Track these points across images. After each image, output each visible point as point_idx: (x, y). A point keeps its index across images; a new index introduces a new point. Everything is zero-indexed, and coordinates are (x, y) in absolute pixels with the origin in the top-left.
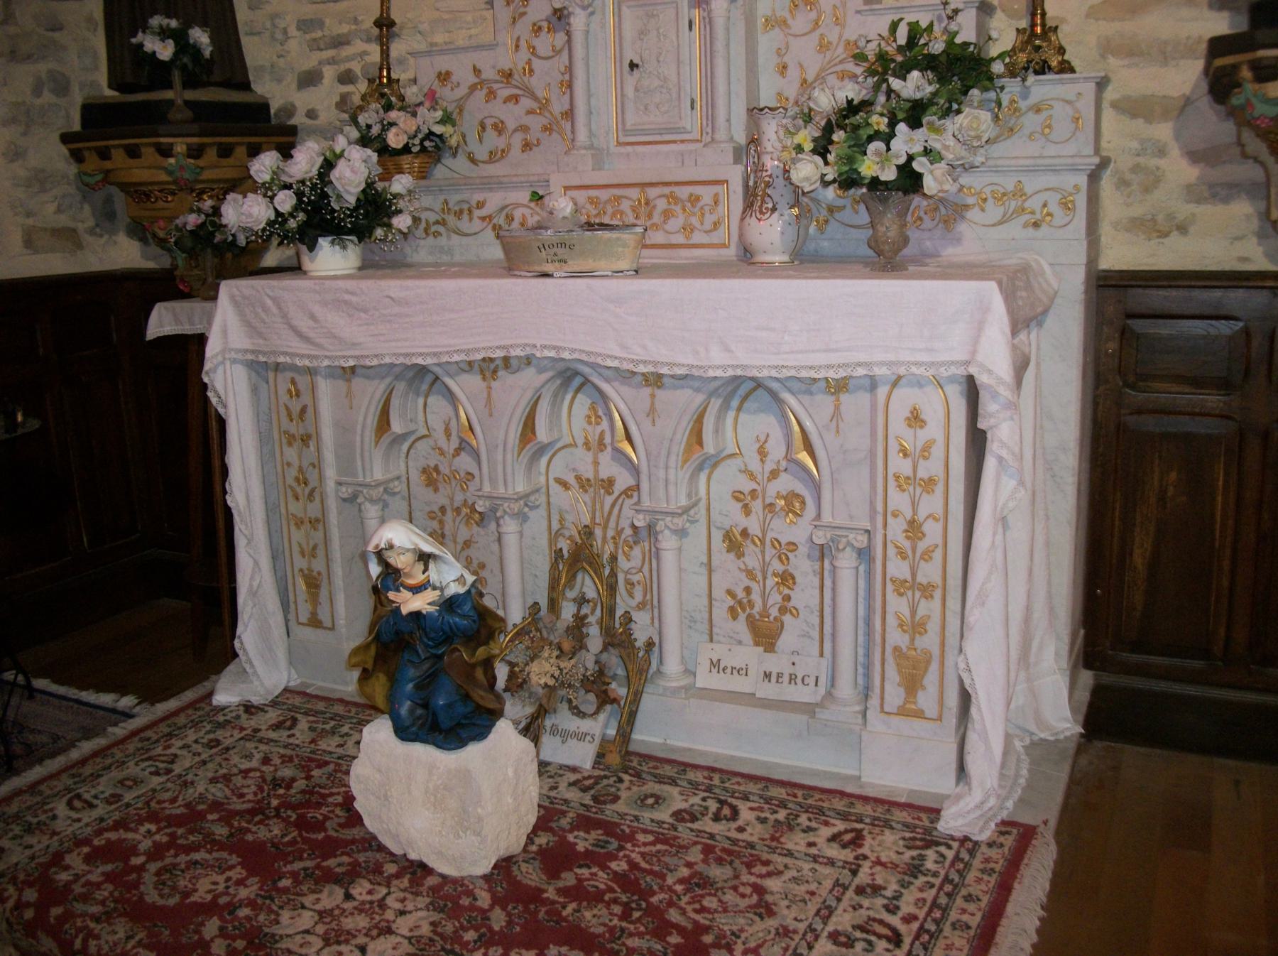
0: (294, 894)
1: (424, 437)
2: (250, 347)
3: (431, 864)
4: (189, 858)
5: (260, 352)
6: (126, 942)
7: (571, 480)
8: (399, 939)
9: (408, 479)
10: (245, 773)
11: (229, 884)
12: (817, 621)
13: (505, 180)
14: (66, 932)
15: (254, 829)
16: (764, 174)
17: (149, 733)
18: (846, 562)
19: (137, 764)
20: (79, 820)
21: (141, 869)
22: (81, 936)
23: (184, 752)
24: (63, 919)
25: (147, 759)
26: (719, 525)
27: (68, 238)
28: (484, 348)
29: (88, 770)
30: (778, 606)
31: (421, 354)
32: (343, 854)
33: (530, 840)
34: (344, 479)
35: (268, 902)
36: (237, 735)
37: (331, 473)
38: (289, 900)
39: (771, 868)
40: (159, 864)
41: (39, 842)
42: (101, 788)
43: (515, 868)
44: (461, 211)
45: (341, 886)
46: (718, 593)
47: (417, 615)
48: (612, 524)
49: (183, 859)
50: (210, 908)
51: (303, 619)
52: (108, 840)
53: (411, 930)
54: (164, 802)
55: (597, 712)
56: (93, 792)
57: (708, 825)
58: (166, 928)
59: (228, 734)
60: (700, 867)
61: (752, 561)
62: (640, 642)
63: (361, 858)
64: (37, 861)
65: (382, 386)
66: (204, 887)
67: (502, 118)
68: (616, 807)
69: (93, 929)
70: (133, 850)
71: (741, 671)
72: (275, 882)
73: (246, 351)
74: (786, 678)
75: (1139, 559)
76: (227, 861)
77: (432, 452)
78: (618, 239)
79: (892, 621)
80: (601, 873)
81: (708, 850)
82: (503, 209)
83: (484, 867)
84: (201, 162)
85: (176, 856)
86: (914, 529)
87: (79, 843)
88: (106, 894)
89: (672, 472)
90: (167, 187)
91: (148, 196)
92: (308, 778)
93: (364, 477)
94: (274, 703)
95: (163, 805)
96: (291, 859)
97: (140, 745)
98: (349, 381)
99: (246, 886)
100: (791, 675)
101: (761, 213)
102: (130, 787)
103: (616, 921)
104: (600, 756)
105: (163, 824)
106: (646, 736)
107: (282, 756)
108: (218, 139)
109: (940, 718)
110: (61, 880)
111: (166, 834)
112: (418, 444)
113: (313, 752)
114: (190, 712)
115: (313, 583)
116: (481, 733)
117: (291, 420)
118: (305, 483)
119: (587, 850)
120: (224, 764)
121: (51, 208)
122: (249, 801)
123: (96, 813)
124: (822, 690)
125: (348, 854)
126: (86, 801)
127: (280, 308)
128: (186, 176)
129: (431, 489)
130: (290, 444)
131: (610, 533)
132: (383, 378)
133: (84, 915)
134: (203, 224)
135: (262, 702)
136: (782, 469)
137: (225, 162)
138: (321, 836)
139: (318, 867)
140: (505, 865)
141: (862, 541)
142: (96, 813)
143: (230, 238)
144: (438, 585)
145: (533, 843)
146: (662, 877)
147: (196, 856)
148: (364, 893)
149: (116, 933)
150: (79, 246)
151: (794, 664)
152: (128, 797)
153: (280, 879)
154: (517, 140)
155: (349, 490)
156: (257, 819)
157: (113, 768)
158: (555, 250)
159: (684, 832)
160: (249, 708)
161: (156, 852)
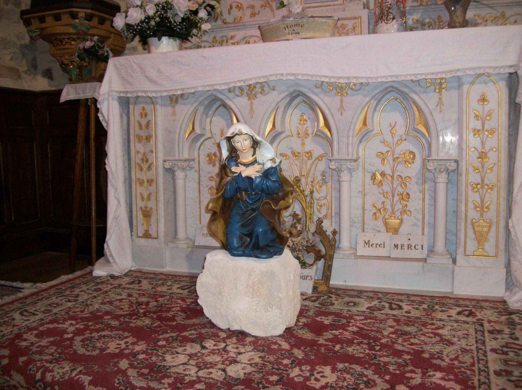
0: (169, 348)
1: (209, 138)
2: (122, 90)
3: (247, 330)
4: (99, 334)
5: (128, 92)
6: (71, 372)
7: (289, 153)
8: (243, 365)
9: (199, 161)
10: (121, 300)
11: (128, 344)
12: (420, 216)
13: (247, 24)
14: (30, 370)
15: (134, 321)
16: (387, 4)
17: (60, 287)
18: (442, 178)
19: (57, 298)
20: (29, 320)
21: (71, 339)
22: (40, 371)
23: (83, 293)
24: (27, 363)
25: (62, 296)
26: (369, 171)
27: (15, 73)
28: (254, 78)
29: (29, 301)
30: (400, 210)
31: (218, 84)
32: (191, 330)
33: (298, 321)
34: (167, 158)
35: (155, 351)
36: (109, 287)
37: (161, 156)
38: (168, 350)
39: (436, 326)
40: (82, 337)
41: (6, 329)
42: (38, 307)
43: (295, 332)
44: (223, 41)
45: (197, 343)
46: (368, 206)
47: (249, 178)
48: (311, 175)
49: (95, 334)
50: (121, 355)
51: (140, 234)
52: (48, 328)
53: (249, 361)
54: (77, 312)
55: (312, 265)
56: (34, 309)
57: (387, 311)
58: (95, 365)
59: (105, 286)
60: (397, 327)
61: (386, 188)
62: (329, 233)
63: (203, 331)
64: (6, 337)
65: (192, 108)
66: (113, 347)
67: (241, 2)
68: (334, 307)
69: (48, 367)
70: (65, 331)
71: (382, 245)
72: (155, 343)
73: (118, 92)
74: (406, 247)
76: (123, 335)
77: (213, 145)
78: (326, 22)
79: (471, 206)
80: (345, 332)
81: (397, 321)
82: (245, 38)
83: (280, 330)
84: (91, 24)
85: (91, 333)
86: (482, 156)
87: (30, 329)
88: (53, 351)
89: (350, 138)
90: (72, 36)
91: (61, 41)
92: (157, 301)
93: (179, 157)
94: (126, 275)
95: (77, 313)
96: (160, 333)
97: (57, 291)
98: (174, 107)
99: (138, 345)
100: (408, 245)
101: (387, 20)
102: (55, 307)
103: (367, 351)
104: (315, 288)
105: (79, 321)
106: (335, 282)
107: (138, 294)
108: (99, 14)
109: (496, 256)
110: (22, 346)
111: (83, 325)
112: (206, 143)
113: (155, 292)
114: (81, 279)
115: (147, 214)
116: (280, 252)
117: (141, 129)
118: (146, 161)
119: (330, 324)
120: (106, 297)
121: (8, 58)
122: (126, 311)
123: (37, 318)
124: (425, 251)
125: (195, 330)
126: (30, 313)
127: (141, 68)
128: (83, 29)
129: (211, 165)
130: (140, 141)
131: (310, 180)
132: (192, 104)
133: (41, 360)
134: (94, 46)
135: (120, 275)
136: (403, 139)
137: (100, 26)
138: (175, 323)
139: (178, 336)
140: (288, 330)
141: (453, 166)
142: (37, 318)
143: (106, 54)
144: (261, 162)
145: (299, 322)
146: (381, 332)
147: (103, 333)
148: (212, 346)
149: (64, 368)
150: (20, 77)
151: (409, 239)
152: (55, 310)
153: (158, 341)
154: (248, 12)
155: (171, 164)
156: (134, 317)
157: (43, 299)
158: (294, 28)
159: (376, 313)
160: (113, 277)
161: (78, 332)
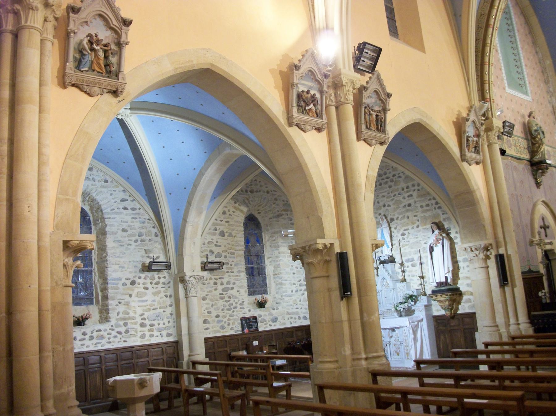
75: (441, 347)
